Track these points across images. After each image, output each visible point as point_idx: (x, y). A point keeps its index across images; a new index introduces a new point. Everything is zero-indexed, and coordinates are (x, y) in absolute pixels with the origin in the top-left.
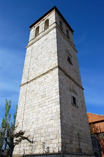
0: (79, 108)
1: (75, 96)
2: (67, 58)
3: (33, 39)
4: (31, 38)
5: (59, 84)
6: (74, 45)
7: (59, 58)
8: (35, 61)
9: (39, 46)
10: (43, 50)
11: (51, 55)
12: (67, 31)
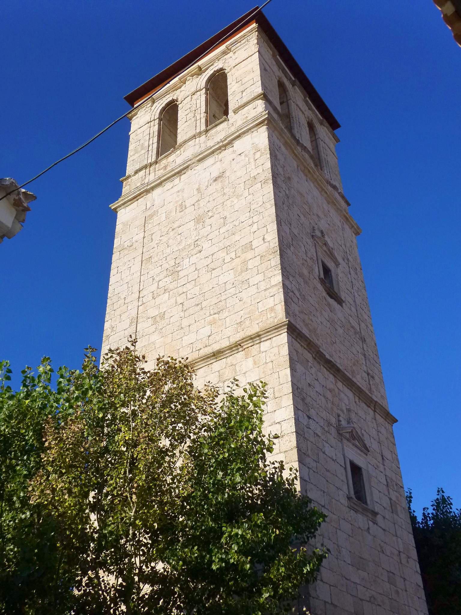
0: (379, 518)
1: (360, 461)
2: (318, 271)
3: (151, 165)
4: (133, 163)
5: (296, 409)
6: (343, 197)
7: (287, 283)
8: (166, 282)
9: (182, 208)
10: (204, 232)
11: (250, 265)
12: (311, 126)
